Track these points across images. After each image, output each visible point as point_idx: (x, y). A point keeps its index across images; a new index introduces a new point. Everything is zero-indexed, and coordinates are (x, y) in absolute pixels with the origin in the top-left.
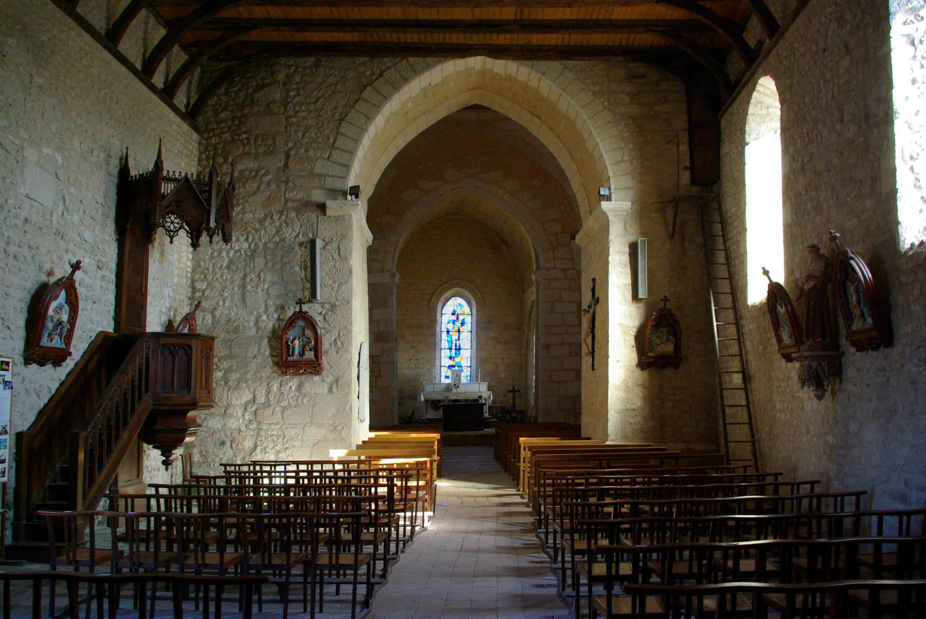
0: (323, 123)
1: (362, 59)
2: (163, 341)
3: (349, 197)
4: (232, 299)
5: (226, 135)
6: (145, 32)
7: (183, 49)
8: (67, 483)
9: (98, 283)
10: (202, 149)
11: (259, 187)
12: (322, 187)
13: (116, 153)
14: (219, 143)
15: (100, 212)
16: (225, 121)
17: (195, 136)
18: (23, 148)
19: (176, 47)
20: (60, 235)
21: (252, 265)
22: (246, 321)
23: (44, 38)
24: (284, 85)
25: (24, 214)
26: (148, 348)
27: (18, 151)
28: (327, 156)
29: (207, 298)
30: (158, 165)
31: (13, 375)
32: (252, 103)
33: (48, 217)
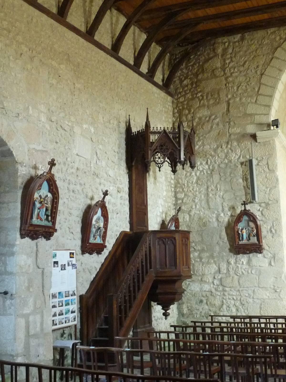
0: (250, 78)
1: (272, 30)
2: (159, 235)
3: (272, 128)
4: (201, 204)
5: (188, 95)
6: (134, 39)
7: (157, 44)
8: (107, 327)
9: (119, 201)
10: (175, 106)
11: (212, 127)
12: (252, 123)
13: (123, 120)
14: (184, 101)
15: (117, 157)
16: (187, 86)
17: (169, 98)
18: (73, 127)
19: (154, 44)
20: (96, 175)
21: (211, 180)
22: (211, 218)
23: (79, 60)
24: (222, 56)
25: (76, 165)
26: (150, 241)
27: (70, 130)
28: (254, 101)
29: (185, 204)
30: (147, 125)
31: (76, 261)
32: (203, 71)
33: (89, 165)
